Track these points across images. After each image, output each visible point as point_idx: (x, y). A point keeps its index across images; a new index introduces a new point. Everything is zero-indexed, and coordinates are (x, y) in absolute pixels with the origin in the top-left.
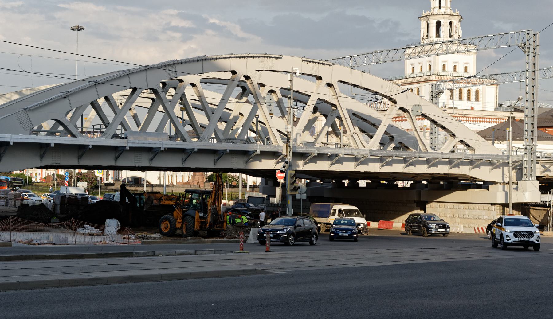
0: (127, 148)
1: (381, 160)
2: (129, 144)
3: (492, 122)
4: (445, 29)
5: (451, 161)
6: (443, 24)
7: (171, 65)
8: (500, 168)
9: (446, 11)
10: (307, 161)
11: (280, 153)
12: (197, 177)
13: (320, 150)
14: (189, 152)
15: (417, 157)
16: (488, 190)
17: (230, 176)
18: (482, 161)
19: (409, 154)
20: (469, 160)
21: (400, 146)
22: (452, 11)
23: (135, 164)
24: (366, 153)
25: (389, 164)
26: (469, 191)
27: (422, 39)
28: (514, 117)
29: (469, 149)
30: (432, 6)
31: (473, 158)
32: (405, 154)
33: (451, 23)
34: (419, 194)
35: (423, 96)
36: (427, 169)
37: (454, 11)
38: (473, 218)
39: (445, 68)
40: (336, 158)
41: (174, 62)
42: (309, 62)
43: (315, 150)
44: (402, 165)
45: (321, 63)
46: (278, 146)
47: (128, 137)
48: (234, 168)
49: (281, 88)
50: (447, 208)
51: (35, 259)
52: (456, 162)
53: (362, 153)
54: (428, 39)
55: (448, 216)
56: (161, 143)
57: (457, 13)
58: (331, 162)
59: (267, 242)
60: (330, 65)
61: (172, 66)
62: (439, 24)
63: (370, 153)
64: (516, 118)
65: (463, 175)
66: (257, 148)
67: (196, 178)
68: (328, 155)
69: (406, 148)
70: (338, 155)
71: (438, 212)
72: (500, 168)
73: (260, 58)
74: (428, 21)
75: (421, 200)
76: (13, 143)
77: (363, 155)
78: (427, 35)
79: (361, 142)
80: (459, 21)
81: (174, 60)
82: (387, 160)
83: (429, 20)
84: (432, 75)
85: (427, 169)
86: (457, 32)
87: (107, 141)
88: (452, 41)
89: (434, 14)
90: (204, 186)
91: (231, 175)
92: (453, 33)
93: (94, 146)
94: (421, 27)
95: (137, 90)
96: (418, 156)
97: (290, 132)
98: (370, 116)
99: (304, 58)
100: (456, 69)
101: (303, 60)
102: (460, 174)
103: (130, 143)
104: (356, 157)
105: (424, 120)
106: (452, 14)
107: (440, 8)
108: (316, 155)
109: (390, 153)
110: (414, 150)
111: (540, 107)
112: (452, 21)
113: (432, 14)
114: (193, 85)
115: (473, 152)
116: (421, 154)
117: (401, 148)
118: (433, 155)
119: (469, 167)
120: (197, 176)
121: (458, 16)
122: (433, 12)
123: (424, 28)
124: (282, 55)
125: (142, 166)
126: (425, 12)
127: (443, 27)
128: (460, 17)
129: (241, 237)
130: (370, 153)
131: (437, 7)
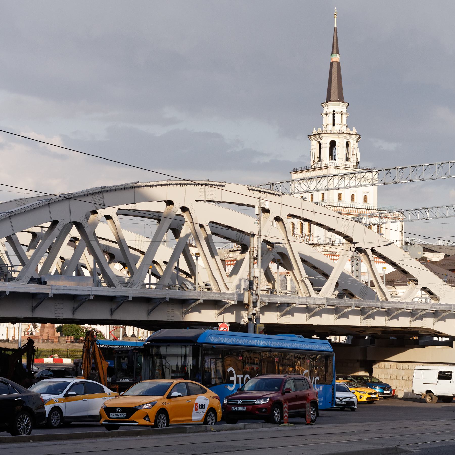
0: (51, 296)
1: (336, 311)
2: (52, 290)
3: (379, 262)
4: (340, 150)
5: (414, 312)
6: (338, 144)
7: (98, 192)
8: (233, 313)
9: (341, 129)
10: (222, 311)
11: (224, 302)
12: (46, 330)
13: (270, 298)
14: (81, 300)
15: (378, 307)
16: (453, 347)
17: (84, 328)
18: (450, 312)
19: (370, 303)
20: (333, 307)
21: (344, 294)
22: (348, 129)
23: (56, 315)
24: (322, 303)
25: (345, 316)
26: (427, 348)
27: (312, 162)
28: (426, 258)
29: (432, 298)
30: (325, 123)
31: (441, 308)
32: (366, 303)
33: (347, 144)
34: (364, 351)
35: (383, 234)
36: (279, 318)
37: (351, 130)
38: (391, 379)
39: (341, 197)
40: (288, 309)
41: (103, 190)
42: (255, 192)
43: (266, 298)
44: (360, 316)
45: (269, 193)
46: (220, 294)
47: (47, 282)
48: (58, 318)
49: (211, 222)
50: (401, 369)
51: (95, 437)
52: (420, 314)
53: (318, 302)
54: (320, 162)
55: (401, 378)
56: (90, 290)
57: (354, 131)
58: (280, 313)
59: (308, 413)
60: (279, 195)
61: (99, 194)
62: (333, 144)
63: (326, 302)
64: (427, 259)
65: (427, 329)
66: (200, 296)
67: (45, 331)
68: (277, 305)
69: (351, 295)
70: (290, 304)
71: (388, 373)
72: (232, 313)
73: (200, 186)
74: (320, 141)
75: (367, 359)
76: (9, 293)
77: (318, 305)
78: (319, 157)
79: (225, 284)
80: (357, 141)
81: (102, 187)
82: (345, 311)
83: (321, 139)
84: (327, 206)
85: (279, 318)
86: (354, 154)
87: (27, 287)
88: (403, 168)
89: (328, 132)
90: (59, 341)
91: (84, 327)
92: (350, 155)
93: (11, 293)
94: (311, 147)
95: (58, 224)
96: (380, 307)
97: (258, 277)
98: (310, 257)
99: (251, 186)
100: (366, 200)
101: (249, 189)
102: (424, 327)
103: (54, 289)
104: (308, 307)
105: (385, 263)
106: (348, 133)
107: (334, 125)
108: (267, 304)
109: (349, 302)
110: (360, 298)
111: (444, 245)
112: (349, 141)
113: (325, 132)
114: (108, 217)
115: (436, 302)
116: (383, 304)
117: (344, 296)
118: (396, 305)
119: (433, 319)
120: (47, 328)
121: (355, 136)
122: (326, 129)
123: (315, 149)
124: (225, 182)
125: (64, 318)
126: (316, 130)
127: (338, 148)
128: (358, 136)
129: (286, 407)
130: (326, 302)
131: (330, 124)
